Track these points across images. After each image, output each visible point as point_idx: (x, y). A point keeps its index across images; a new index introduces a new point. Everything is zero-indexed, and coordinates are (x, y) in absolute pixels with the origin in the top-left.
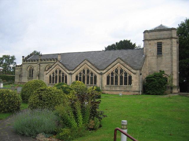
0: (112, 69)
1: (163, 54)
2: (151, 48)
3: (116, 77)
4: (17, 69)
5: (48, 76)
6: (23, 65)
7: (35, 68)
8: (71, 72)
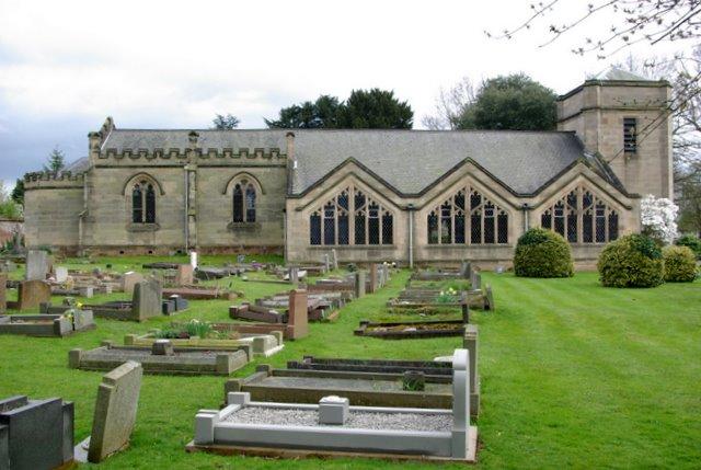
5: (306, 216)
7: (169, 187)
8: (410, 201)
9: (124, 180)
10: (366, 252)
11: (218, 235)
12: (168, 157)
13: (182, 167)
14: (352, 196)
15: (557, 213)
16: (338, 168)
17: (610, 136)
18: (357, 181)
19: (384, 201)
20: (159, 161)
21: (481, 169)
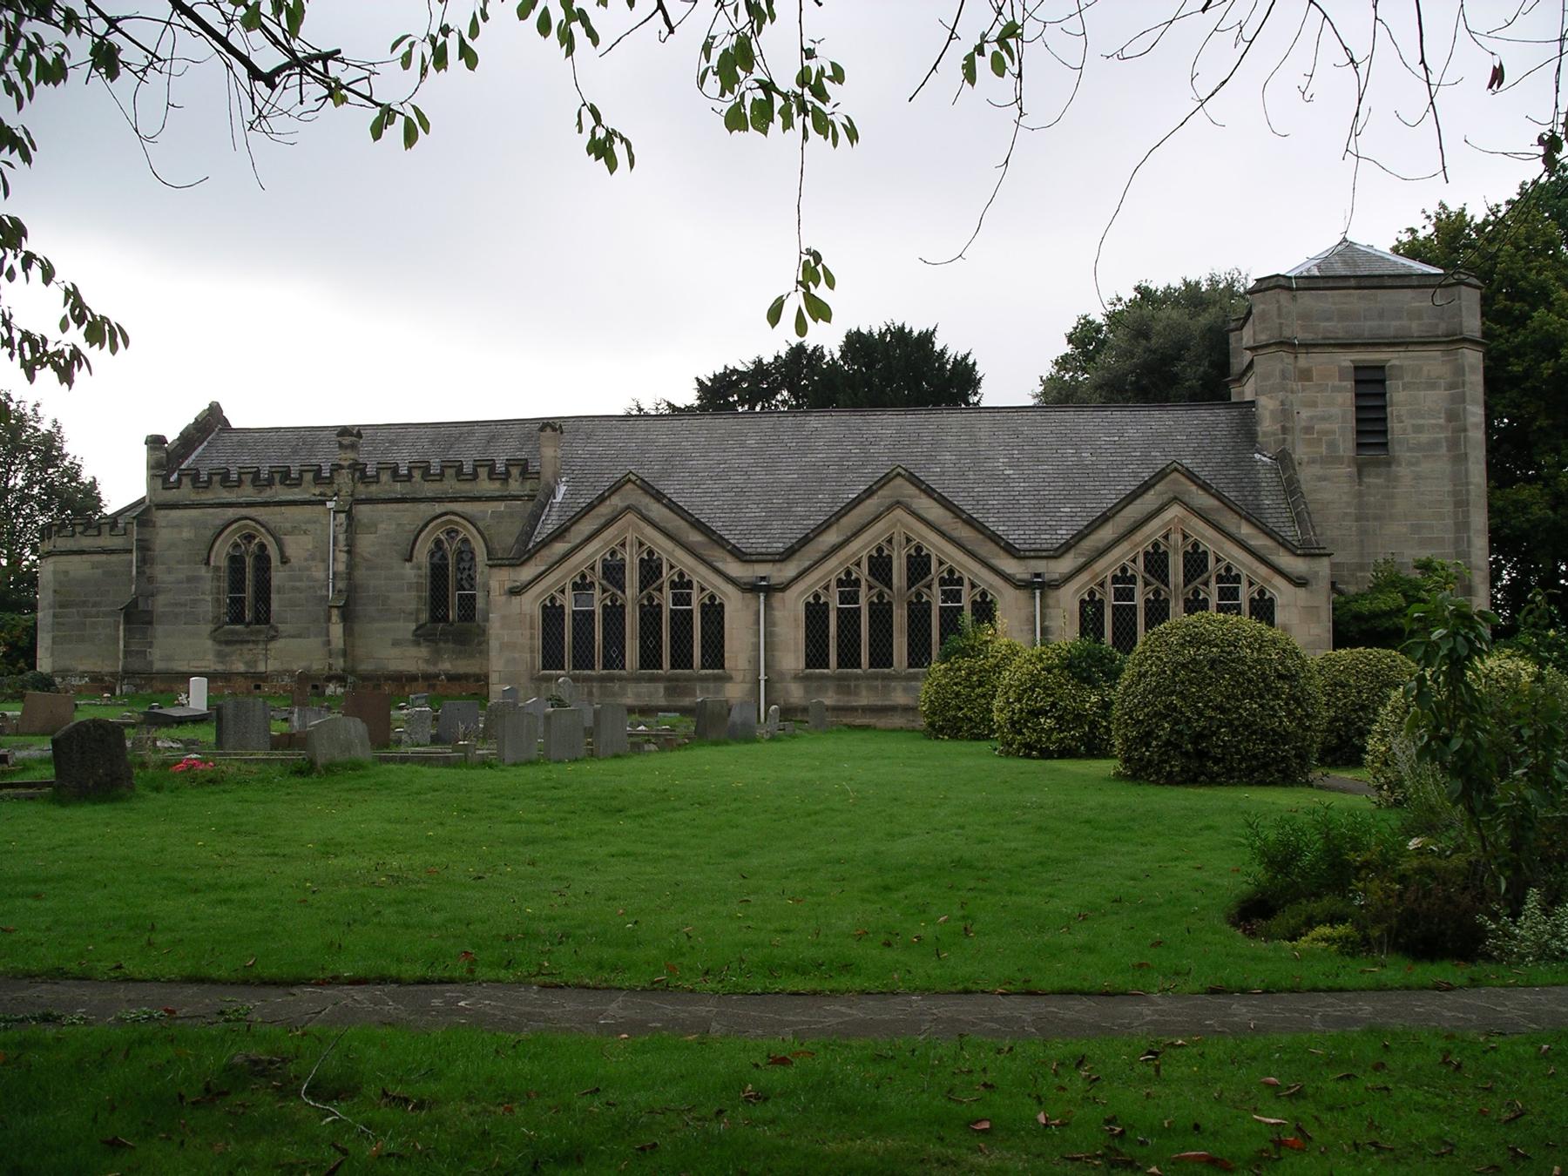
0: (1125, 546)
1: (1398, 451)
2: (1314, 404)
3: (881, 614)
4: (81, 552)
5: (530, 604)
6: (161, 516)
7: (297, 547)
8: (762, 570)
9: (209, 533)
10: (661, 687)
11: (395, 652)
12: (298, 483)
13: (323, 503)
14: (631, 559)
15: (1119, 595)
16: (602, 499)
17: (1319, 411)
18: (642, 524)
19: (702, 570)
20: (451, 485)
21: (929, 492)
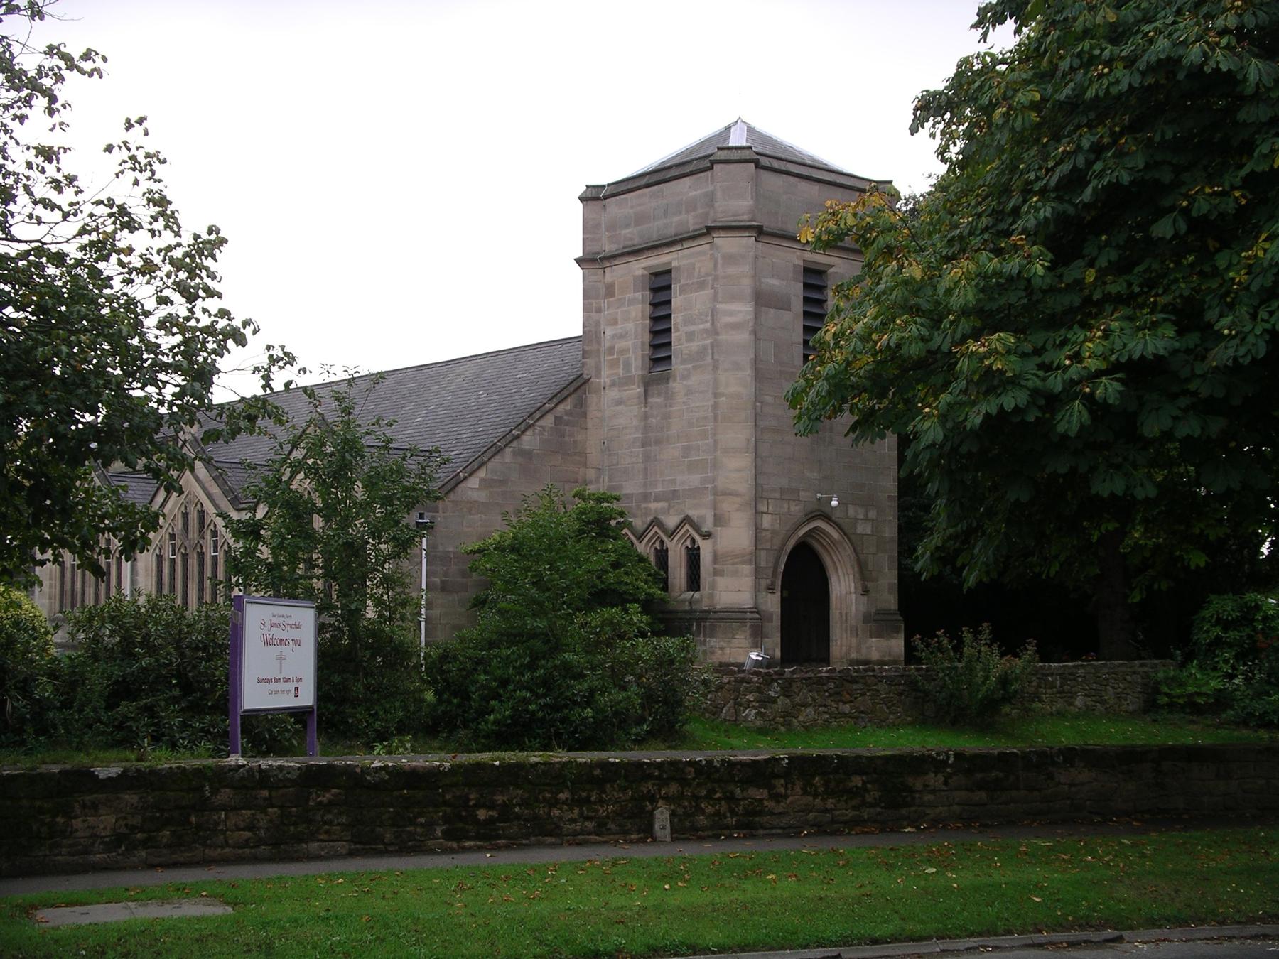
2: (614, 322)
